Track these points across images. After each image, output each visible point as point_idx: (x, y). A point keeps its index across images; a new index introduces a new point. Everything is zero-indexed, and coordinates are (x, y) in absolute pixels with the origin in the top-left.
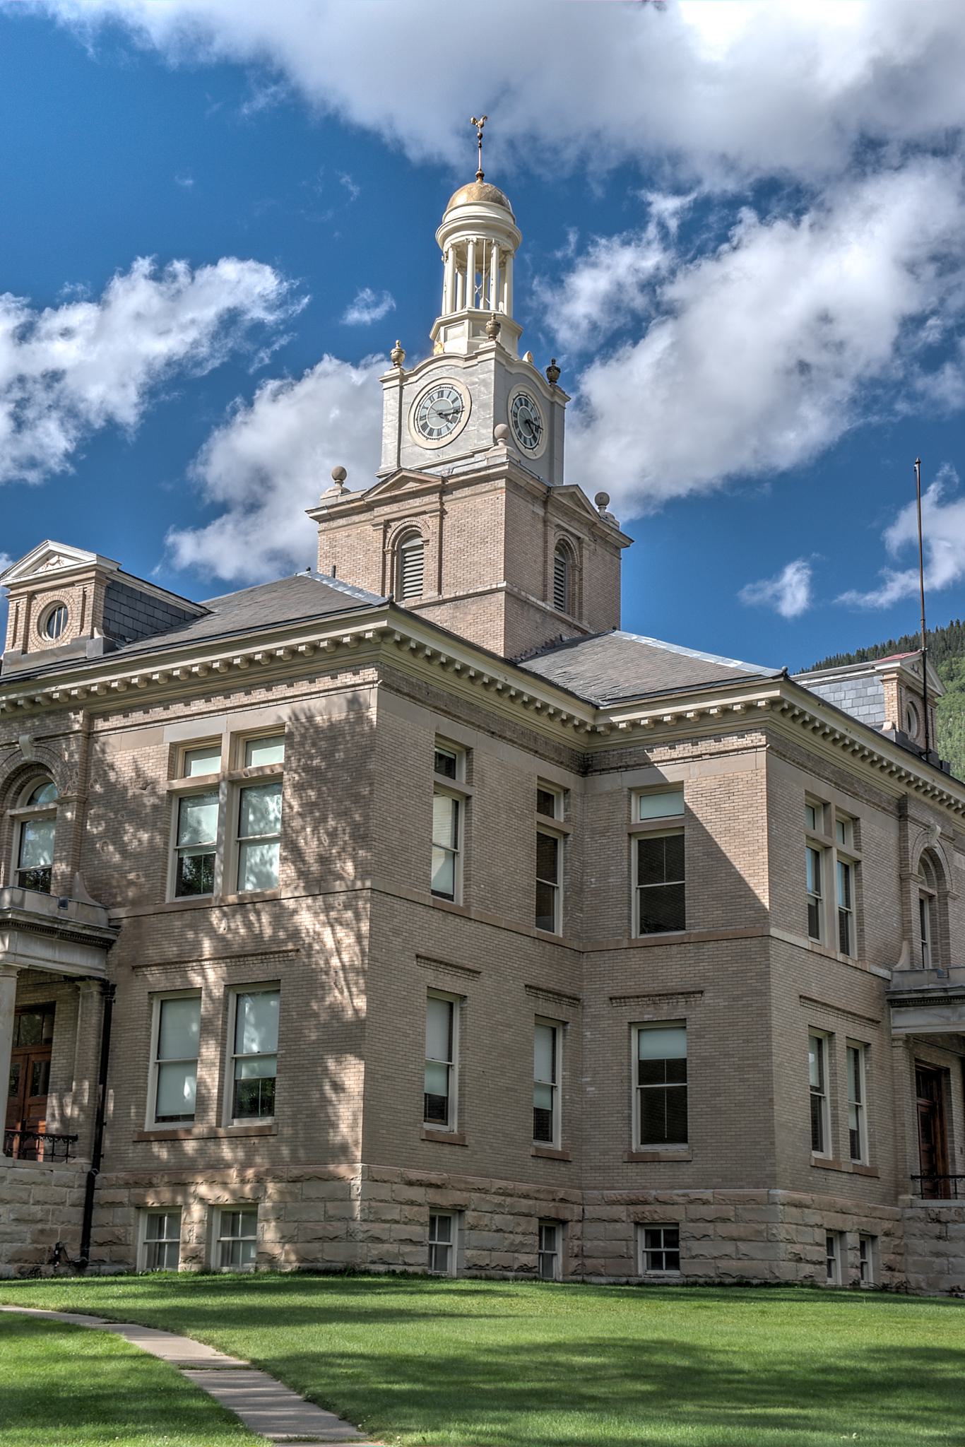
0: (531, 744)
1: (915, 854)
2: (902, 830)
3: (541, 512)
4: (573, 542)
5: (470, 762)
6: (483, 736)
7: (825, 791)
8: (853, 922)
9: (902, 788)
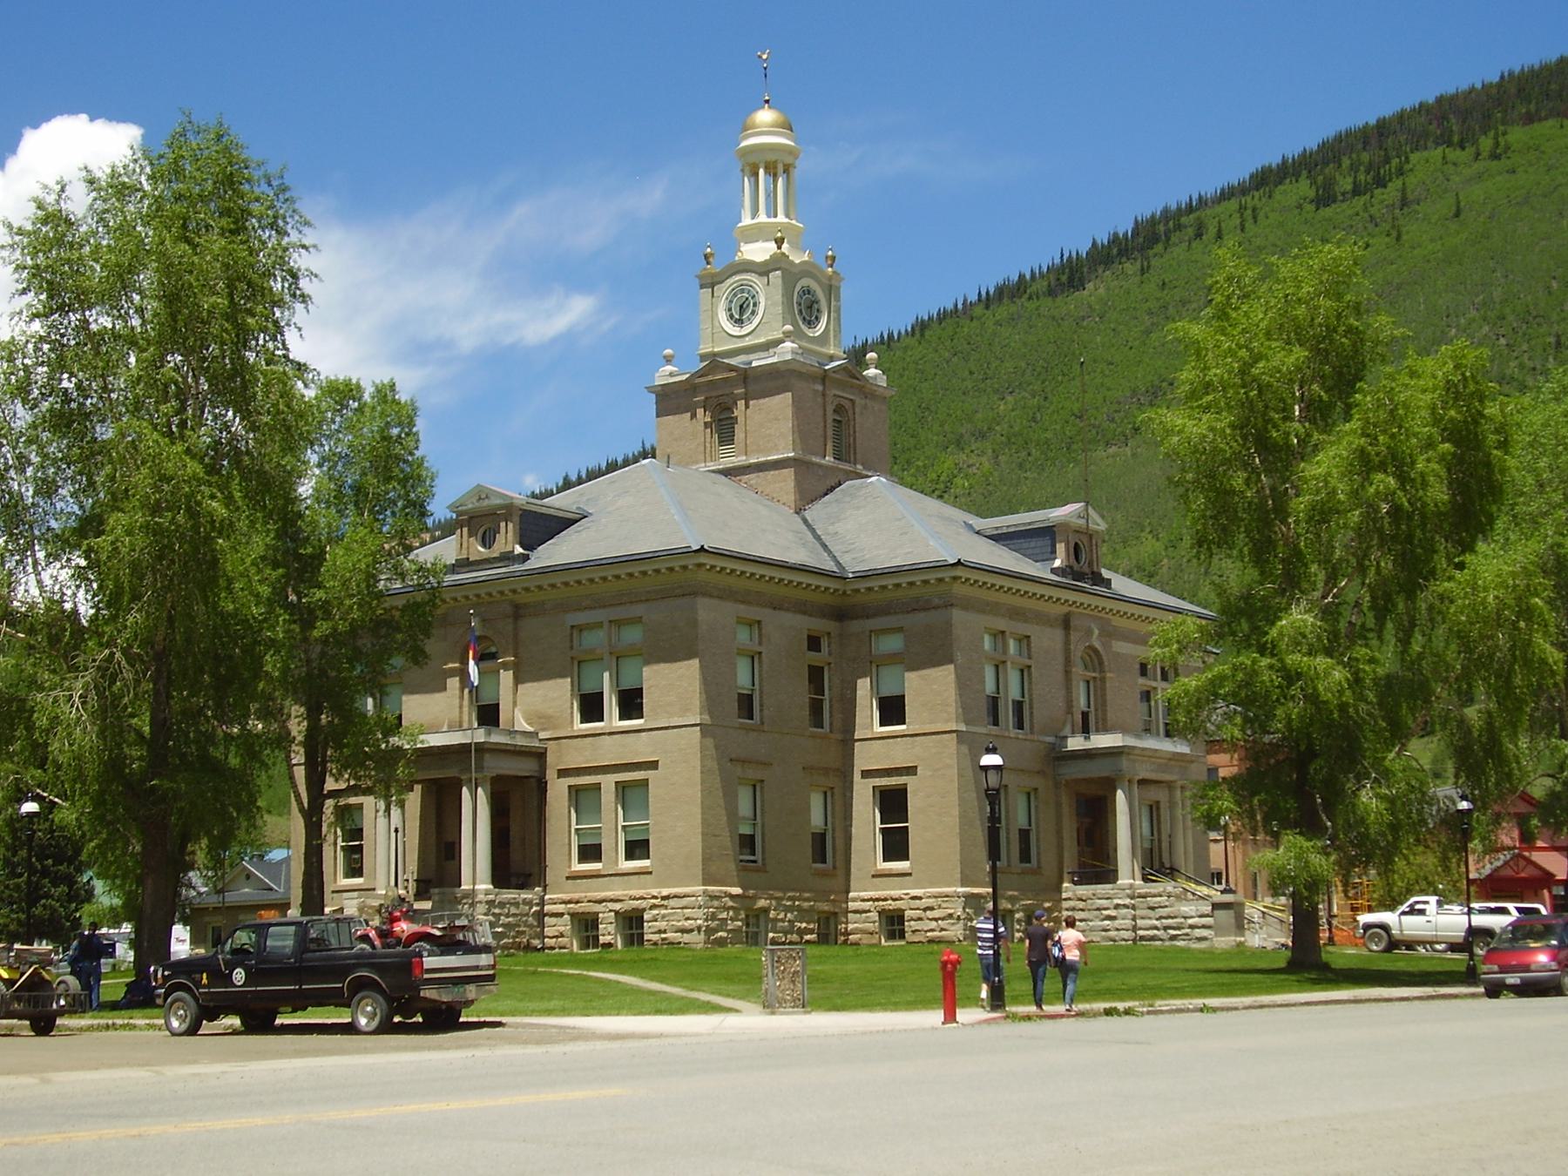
0: (802, 608)
1: (1078, 651)
2: (1067, 635)
3: (820, 388)
4: (847, 404)
5: (760, 629)
6: (768, 611)
7: (1001, 624)
8: (1026, 707)
9: (1066, 609)
